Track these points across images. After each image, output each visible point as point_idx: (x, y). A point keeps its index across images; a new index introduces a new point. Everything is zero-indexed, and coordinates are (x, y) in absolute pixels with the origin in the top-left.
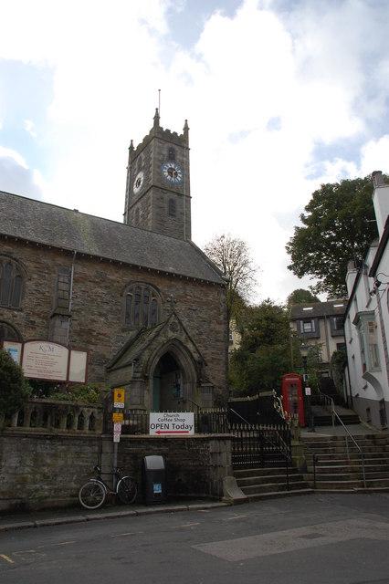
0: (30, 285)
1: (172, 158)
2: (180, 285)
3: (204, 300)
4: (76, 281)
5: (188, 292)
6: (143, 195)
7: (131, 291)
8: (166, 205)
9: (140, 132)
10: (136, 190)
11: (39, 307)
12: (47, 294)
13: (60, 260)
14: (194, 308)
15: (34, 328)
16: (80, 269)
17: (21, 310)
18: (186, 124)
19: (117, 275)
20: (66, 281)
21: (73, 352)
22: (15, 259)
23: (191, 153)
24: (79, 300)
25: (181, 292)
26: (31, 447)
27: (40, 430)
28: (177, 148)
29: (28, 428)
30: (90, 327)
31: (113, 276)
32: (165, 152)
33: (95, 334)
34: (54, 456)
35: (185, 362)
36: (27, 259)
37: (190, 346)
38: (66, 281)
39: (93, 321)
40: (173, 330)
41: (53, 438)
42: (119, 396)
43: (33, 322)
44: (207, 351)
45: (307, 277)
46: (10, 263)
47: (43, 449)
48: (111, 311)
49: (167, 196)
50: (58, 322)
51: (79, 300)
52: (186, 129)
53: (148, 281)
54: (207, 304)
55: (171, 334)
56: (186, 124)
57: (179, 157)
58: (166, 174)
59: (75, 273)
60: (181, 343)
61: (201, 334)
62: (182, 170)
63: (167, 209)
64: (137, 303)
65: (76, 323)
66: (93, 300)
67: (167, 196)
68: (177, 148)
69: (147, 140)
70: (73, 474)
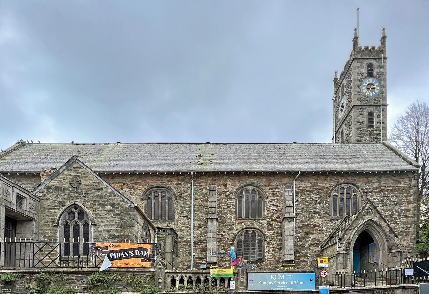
0: (268, 202)
2: (375, 180)
5: (382, 184)
7: (337, 191)
9: (345, 53)
12: (278, 205)
13: (285, 180)
14: (387, 195)
19: (326, 182)
25: (376, 185)
28: (374, 62)
32: (364, 71)
33: (312, 226)
37: (382, 223)
39: (311, 218)
43: (272, 226)
53: (350, 181)
56: (384, 33)
57: (376, 71)
61: (393, 214)
62: (380, 81)
63: (366, 123)
66: (309, 204)
68: (374, 62)
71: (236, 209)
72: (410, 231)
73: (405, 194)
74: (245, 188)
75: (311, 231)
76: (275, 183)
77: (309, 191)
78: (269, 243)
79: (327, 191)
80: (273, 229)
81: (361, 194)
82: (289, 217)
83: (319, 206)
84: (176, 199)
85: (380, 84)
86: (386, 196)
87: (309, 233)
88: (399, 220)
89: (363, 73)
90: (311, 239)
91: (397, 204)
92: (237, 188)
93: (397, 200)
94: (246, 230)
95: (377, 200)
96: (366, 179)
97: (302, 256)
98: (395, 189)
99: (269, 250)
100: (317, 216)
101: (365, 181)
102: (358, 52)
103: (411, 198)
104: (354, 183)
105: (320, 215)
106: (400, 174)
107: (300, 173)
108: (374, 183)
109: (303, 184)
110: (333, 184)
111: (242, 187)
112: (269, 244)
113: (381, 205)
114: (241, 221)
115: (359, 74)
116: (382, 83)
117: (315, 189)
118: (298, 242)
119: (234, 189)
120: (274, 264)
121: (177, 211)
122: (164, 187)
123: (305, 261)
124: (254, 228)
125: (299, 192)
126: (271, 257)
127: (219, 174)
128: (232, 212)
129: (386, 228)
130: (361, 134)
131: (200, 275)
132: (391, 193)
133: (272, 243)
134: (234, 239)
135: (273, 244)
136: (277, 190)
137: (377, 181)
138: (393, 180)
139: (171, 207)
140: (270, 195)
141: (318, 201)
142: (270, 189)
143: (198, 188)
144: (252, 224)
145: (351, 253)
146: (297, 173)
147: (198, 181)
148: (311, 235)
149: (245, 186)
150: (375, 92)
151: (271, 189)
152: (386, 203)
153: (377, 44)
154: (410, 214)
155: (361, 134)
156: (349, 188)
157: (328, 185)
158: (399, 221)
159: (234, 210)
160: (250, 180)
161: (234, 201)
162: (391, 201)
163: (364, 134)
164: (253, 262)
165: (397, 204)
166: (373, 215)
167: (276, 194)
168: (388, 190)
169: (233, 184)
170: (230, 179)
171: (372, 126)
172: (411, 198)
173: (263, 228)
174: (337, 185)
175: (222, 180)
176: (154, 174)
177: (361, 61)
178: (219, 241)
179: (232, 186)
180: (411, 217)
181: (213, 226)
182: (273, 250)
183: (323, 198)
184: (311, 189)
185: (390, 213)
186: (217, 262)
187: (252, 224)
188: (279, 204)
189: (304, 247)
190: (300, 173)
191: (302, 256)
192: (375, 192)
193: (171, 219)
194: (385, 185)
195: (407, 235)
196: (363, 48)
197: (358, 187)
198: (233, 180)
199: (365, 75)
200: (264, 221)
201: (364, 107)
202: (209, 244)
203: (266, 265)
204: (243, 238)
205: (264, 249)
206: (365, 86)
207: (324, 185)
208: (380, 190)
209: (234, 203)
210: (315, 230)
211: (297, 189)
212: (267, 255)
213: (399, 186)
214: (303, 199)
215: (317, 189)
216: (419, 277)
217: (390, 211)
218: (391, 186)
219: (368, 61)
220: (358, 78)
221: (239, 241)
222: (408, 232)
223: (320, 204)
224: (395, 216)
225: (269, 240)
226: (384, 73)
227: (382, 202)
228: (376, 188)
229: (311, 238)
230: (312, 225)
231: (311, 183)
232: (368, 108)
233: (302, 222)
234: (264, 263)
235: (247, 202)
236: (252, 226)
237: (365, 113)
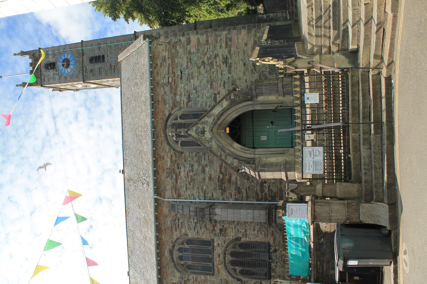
3: (169, 61)
4: (179, 196)
5: (165, 81)
7: (177, 142)
8: (97, 66)
11: (208, 226)
12: (196, 221)
14: (179, 73)
16: (168, 193)
18: (18, 54)
19: (165, 157)
24: (194, 192)
25: (167, 89)
30: (216, 181)
33: (221, 176)
39: (210, 178)
43: (221, 230)
44: (220, 55)
45: (120, 16)
48: (199, 162)
51: (194, 192)
52: (23, 53)
54: (173, 58)
56: (18, 54)
58: (69, 70)
60: (215, 124)
61: (203, 62)
65: (214, 194)
66: (193, 180)
71: (201, 274)
72: (226, 37)
73: (178, 48)
74: (175, 261)
75: (227, 177)
76: (169, 223)
77: (176, 180)
78: (244, 235)
79: (176, 157)
80: (226, 229)
81: (178, 110)
83: (196, 166)
85: (62, 54)
86: (180, 74)
87: (229, 181)
88: (211, 53)
89: (54, 74)
90: (238, 178)
91: (190, 59)
92: (176, 271)
93: (185, 59)
94: (227, 264)
95: (186, 87)
96: (160, 104)
97: (262, 191)
98: (172, 62)
99: (254, 236)
100: (207, 169)
101: (163, 104)
105: (206, 165)
107: (156, 197)
108: (165, 93)
109: (169, 187)
110: (167, 148)
112: (246, 235)
113: (191, 80)
114: (216, 269)
116: (62, 51)
117: (173, 173)
118: (242, 196)
119: (178, 274)
120: (272, 229)
123: (269, 187)
125: (178, 194)
126: (263, 233)
127: (160, 251)
128: (205, 280)
129: (222, 106)
130: (111, 69)
132: (177, 67)
133: (244, 230)
134: (239, 280)
135: (246, 230)
136: (177, 221)
137: (162, 89)
138: (161, 67)
140: (183, 231)
141: (188, 168)
142: (176, 230)
144: (219, 255)
146: (156, 200)
149: (173, 261)
150: (70, 57)
151: (176, 229)
152: (189, 74)
154: (202, 39)
155: (111, 69)
157: (169, 156)
158: (213, 52)
159: (203, 277)
160: (167, 254)
161: (192, 276)
162: (187, 67)
163: (111, 66)
164: (270, 258)
165: (190, 59)
166: (205, 126)
167: (181, 223)
168: (174, 73)
169: (172, 275)
170: (167, 278)
171: (103, 56)
173: (224, 242)
177: (42, 78)
179: (174, 277)
180: (207, 36)
182: (254, 230)
183: (185, 161)
184: (174, 177)
185: (202, 67)
187: (219, 255)
188: (194, 219)
189: (249, 187)
190: (156, 197)
191: (262, 191)
192: (176, 90)
194: (167, 77)
195: (231, 40)
197: (170, 115)
198: (167, 275)
199: (55, 72)
201: (85, 69)
203: (274, 240)
204: (238, 269)
205: (252, 242)
206: (65, 71)
208: (173, 83)
209: (195, 276)
210: (226, 171)
211: (175, 196)
212: (261, 238)
213: (168, 58)
214: (186, 189)
215: (174, 170)
216: (295, 118)
217: (200, 67)
218: (169, 69)
220: (58, 79)
221: (242, 273)
222: (226, 39)
223: (192, 166)
224: (206, 61)
225: (240, 235)
226: (53, 49)
227: (188, 79)
228: (171, 88)
229: (236, 178)
230: (219, 176)
231: (167, 177)
232: (86, 64)
233: (215, 189)
234: (271, 243)
235: (193, 259)
236: (222, 255)
237: (89, 67)
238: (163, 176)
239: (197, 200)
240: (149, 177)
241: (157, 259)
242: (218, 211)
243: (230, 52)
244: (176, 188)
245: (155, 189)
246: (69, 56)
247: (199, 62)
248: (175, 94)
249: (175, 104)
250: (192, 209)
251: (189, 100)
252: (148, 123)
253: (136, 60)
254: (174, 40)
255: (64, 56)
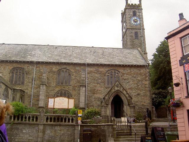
0: (73, 77)
1: (135, 14)
2: (128, 69)
5: (132, 71)
6: (126, 32)
7: (109, 73)
8: (134, 35)
9: (123, 6)
10: (124, 31)
13: (82, 67)
15: (75, 91)
17: (71, 86)
20: (84, 73)
21: (69, 100)
22: (67, 69)
23: (144, 11)
26: (54, 128)
27: (54, 123)
28: (136, 10)
29: (50, 123)
31: (102, 69)
32: (132, 13)
34: (60, 130)
35: (123, 98)
36: (72, 69)
37: (125, 92)
38: (84, 73)
39: (95, 86)
40: (117, 87)
41: (60, 125)
42: (80, 112)
46: (66, 71)
47: (58, 128)
49: (134, 31)
50: (81, 88)
53: (115, 69)
54: (141, 74)
55: (116, 88)
57: (138, 14)
58: (133, 22)
59: (88, 71)
61: (138, 86)
62: (140, 18)
63: (134, 36)
64: (111, 77)
67: (134, 31)
68: (136, 10)
69: (125, 9)
70: (66, 136)
82: (83, 86)
84: (26, 74)
87: (94, 94)
102: (128, 6)
103: (147, 78)
104: (118, 70)
106: (137, 67)
111: (60, 70)
115: (129, 15)
117: (98, 72)
121: (26, 80)
122: (20, 68)
124: (65, 90)
131: (38, 116)
139: (23, 78)
143: (38, 69)
145: (110, 106)
147: (38, 66)
148: (95, 95)
153: (137, 3)
154: (147, 86)
156: (115, 72)
160: (65, 66)
162: (137, 79)
172: (147, 78)
174: (109, 70)
175: (51, 66)
176: (17, 62)
178: (46, 96)
181: (43, 89)
186: (45, 107)
193: (23, 83)
196: (130, 4)
197: (119, 72)
200: (71, 87)
202: (40, 97)
207: (102, 70)
219: (134, 10)
223: (100, 79)
236: (64, 89)
238: (96, 68)
239: (87, 80)
240: (20, 58)
241: (64, 62)
242: (84, 89)
243: (142, 96)
244: (91, 72)
245: (103, 64)
246: (139, 23)
247: (139, 84)
248: (127, 74)
249: (124, 74)
250: (84, 78)
251: (125, 80)
252: (139, 63)
253: (133, 57)
254: (147, 75)
255: (139, 20)
